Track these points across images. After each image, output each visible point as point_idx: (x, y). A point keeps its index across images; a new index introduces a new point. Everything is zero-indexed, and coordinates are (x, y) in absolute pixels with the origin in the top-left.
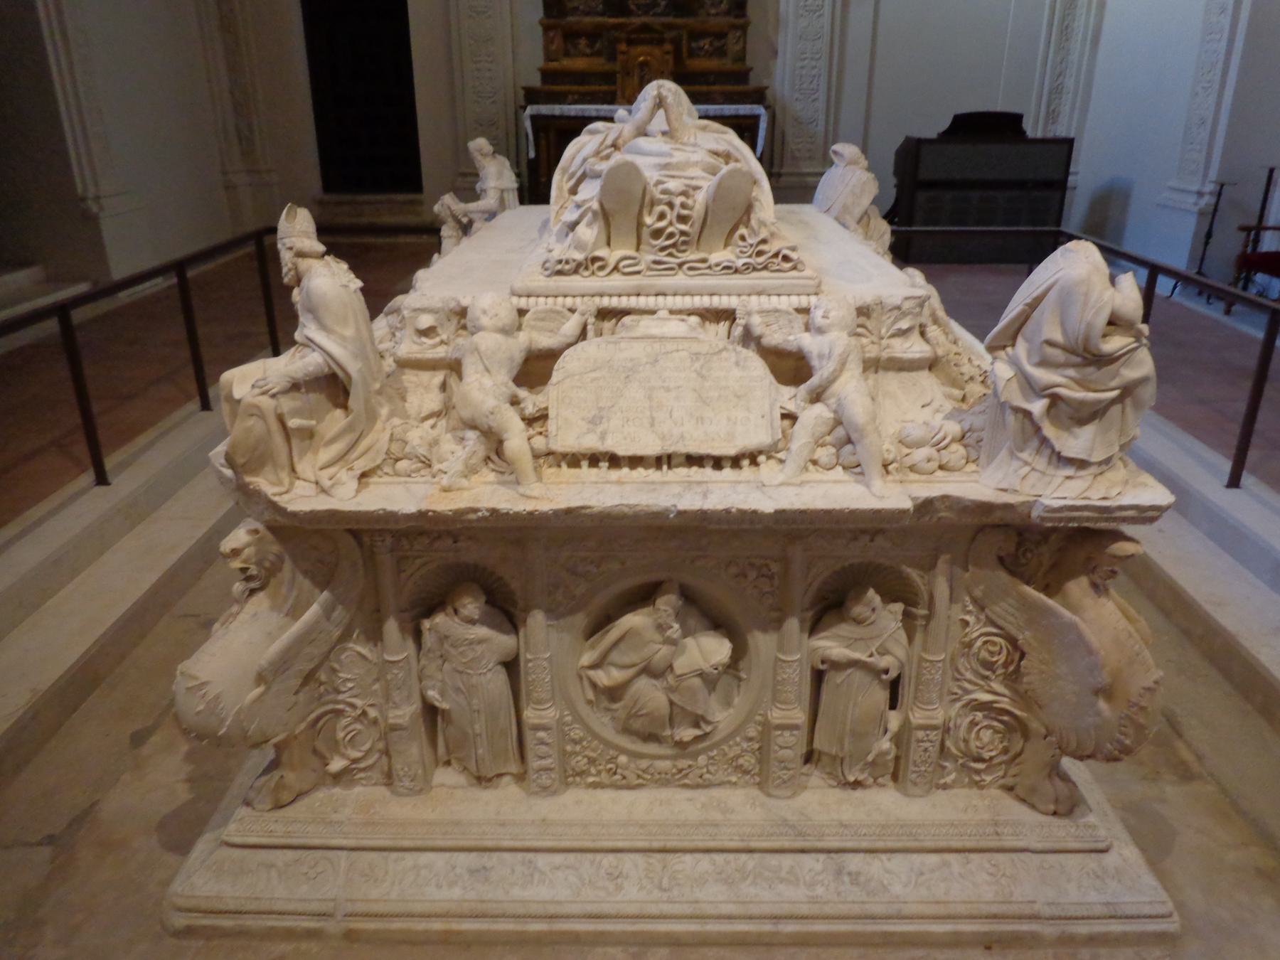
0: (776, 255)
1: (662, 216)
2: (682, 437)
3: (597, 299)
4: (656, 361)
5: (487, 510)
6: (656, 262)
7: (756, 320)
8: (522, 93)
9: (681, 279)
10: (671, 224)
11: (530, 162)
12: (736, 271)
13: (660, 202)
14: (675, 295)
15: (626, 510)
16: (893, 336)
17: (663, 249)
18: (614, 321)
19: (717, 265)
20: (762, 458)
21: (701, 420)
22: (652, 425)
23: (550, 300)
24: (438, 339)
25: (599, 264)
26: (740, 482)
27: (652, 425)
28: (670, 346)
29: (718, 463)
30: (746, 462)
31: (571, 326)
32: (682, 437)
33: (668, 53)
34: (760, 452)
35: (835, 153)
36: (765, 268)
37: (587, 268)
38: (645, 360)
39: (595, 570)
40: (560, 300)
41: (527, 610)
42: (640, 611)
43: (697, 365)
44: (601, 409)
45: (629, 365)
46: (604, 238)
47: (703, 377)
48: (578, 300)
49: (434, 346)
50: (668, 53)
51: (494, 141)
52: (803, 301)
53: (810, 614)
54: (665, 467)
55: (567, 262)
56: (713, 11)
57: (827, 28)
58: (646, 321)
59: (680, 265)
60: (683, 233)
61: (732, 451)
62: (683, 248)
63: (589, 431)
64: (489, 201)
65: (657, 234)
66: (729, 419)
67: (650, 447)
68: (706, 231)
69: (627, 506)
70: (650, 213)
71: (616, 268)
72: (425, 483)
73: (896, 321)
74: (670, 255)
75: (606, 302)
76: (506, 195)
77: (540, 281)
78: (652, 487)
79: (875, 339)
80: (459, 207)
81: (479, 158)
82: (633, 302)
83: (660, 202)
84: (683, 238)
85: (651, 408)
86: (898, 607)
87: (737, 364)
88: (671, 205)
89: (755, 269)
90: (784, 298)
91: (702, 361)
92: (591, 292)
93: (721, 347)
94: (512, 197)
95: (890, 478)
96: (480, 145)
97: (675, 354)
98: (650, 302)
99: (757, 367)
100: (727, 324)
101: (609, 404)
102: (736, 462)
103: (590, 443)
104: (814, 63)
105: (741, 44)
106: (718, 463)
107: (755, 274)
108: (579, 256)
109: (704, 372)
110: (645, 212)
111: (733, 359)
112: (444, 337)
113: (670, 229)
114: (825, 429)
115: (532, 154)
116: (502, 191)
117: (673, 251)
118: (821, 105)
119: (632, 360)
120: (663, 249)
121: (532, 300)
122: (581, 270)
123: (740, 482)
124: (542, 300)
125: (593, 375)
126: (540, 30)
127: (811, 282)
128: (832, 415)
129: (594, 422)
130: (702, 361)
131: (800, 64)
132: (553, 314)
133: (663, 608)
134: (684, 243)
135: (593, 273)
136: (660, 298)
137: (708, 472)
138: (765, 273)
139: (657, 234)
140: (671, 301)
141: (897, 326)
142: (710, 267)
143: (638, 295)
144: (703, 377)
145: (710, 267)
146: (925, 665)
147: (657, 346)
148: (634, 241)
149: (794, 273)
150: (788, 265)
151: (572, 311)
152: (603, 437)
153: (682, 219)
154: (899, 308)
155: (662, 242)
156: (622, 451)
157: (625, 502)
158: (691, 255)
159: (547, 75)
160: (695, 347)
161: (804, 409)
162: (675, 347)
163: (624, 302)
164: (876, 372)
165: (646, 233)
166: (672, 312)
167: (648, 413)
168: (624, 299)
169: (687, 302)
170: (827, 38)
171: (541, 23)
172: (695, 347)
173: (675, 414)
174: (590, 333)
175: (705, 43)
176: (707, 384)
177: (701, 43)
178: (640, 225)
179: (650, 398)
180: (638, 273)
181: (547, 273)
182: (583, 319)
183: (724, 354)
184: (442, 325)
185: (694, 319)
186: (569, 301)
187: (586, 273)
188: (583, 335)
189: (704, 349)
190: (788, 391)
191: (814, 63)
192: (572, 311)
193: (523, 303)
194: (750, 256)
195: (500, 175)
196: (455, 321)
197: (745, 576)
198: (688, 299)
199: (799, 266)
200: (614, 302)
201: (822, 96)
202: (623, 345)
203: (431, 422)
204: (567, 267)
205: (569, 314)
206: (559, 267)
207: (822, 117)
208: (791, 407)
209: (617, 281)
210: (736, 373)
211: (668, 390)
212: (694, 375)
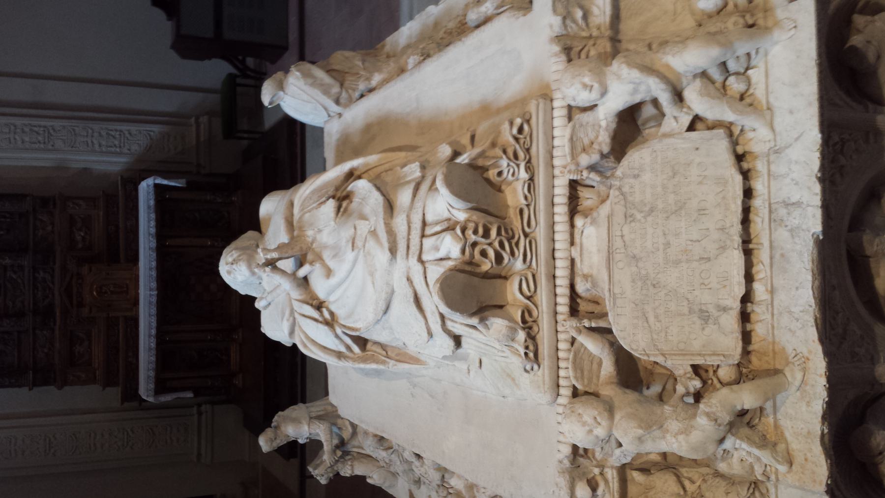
0: (517, 139)
1: (484, 254)
2: (722, 229)
3: (560, 318)
4: (634, 257)
5: (823, 424)
6: (525, 260)
7: (585, 160)
8: (126, 404)
9: (540, 233)
10: (490, 244)
11: (196, 395)
12: (531, 179)
13: (472, 256)
14: (553, 240)
15: (817, 283)
16: (587, 25)
17: (512, 254)
18: (579, 300)
19: (526, 198)
20: (740, 150)
21: (701, 211)
22: (709, 259)
23: (562, 364)
24: (599, 479)
25: (526, 315)
26: (769, 171)
27: (709, 259)
28: (618, 243)
29: (748, 193)
30: (745, 165)
31: (593, 346)
32: (722, 229)
33: (90, 270)
34: (735, 151)
35: (270, 103)
36: (528, 150)
37: (530, 328)
38: (634, 269)
39: (840, 315)
40: (561, 354)
41: (874, 382)
42: (874, 271)
43: (639, 216)
44: (691, 311)
45: (639, 284)
46: (498, 311)
47: (652, 210)
48: (561, 336)
49: (606, 481)
50: (90, 270)
51: (258, 431)
52: (559, 114)
53: (871, 106)
54: (751, 246)
55: (527, 348)
56: (49, 228)
57: (65, 123)
58: (582, 267)
59: (526, 235)
60: (499, 233)
61: (739, 178)
62: (510, 232)
63: (716, 322)
64: (320, 431)
65: (499, 258)
66: (700, 183)
67: (737, 258)
68: (491, 210)
69: (813, 282)
70: (478, 266)
71: (529, 298)
72: (776, 487)
73: (574, 21)
74: (517, 244)
75: (563, 308)
76: (313, 415)
77: (544, 372)
78: (777, 256)
79: (591, 42)
80: (326, 457)
81: (278, 441)
82: (562, 282)
83: (472, 256)
84: (503, 233)
85: (688, 261)
86: (859, 20)
87: (636, 177)
88: (474, 244)
89: (529, 161)
90: (556, 133)
91: (634, 212)
92: (554, 322)
93: (617, 193)
94: (316, 407)
95: (761, 22)
96: (265, 443)
97: (626, 238)
98: (562, 265)
99: (636, 157)
100: (579, 188)
101: (685, 303)
102: (746, 175)
103: (731, 321)
104: (96, 134)
105: (81, 202)
106: (748, 193)
107: (534, 161)
108: (521, 335)
109: (647, 209)
110: (478, 270)
111: (632, 181)
112: (596, 471)
113: (496, 244)
114: (711, 87)
115: (190, 395)
116: (311, 418)
117: (514, 242)
118: (134, 128)
119: (633, 281)
120: (512, 254)
121: (562, 382)
122: (533, 334)
123: (769, 171)
124: (562, 373)
125: (652, 319)
126: (67, 388)
127: (541, 106)
128: (698, 81)
129: (705, 317)
130: (634, 212)
131: (97, 146)
132: (577, 365)
133: (875, 248)
134: (506, 231)
135: (534, 321)
136: (558, 254)
137: (757, 203)
138: (533, 151)
139: (499, 258)
140: (561, 242)
141: (580, 21)
142: (528, 205)
143: (554, 277)
144: (652, 210)
145: (528, 205)
146: (239, 89)
147: (618, 257)
148: (499, 281)
149: (533, 121)
150: (526, 127)
151: (573, 341)
152: (725, 309)
153: (486, 235)
154: (564, 18)
155: (506, 257)
156: (740, 291)
157: (810, 285)
158: (517, 224)
159: (109, 382)
160: (619, 218)
161: (689, 108)
162: (619, 239)
163: (563, 291)
164: (620, 41)
165: (497, 270)
166: (572, 243)
167: (695, 264)
168: (559, 291)
169: (562, 228)
170: (74, 123)
171: (60, 388)
172: (619, 218)
173: (695, 237)
174: (602, 324)
175: (79, 236)
176: (661, 206)
177: (79, 238)
178: (486, 276)
179: (677, 263)
180: (534, 276)
181: (536, 367)
182: (584, 331)
183: (626, 189)
184: (584, 474)
185: (579, 222)
186: (562, 346)
187: (535, 329)
188: (605, 332)
189: (620, 210)
190: (669, 124)
191: (96, 134)
192: (573, 341)
193: (566, 392)
194: (518, 166)
195: (296, 421)
196: (581, 460)
197: (842, 167)
198: (557, 228)
199: (527, 117)
200: (563, 301)
201: (124, 127)
202: (617, 290)
203: (687, 483)
204: (531, 347)
205: (576, 344)
206: (531, 355)
207: (148, 127)
208: (686, 120)
209: (543, 297)
210: (647, 177)
211: (668, 245)
212: (650, 219)
